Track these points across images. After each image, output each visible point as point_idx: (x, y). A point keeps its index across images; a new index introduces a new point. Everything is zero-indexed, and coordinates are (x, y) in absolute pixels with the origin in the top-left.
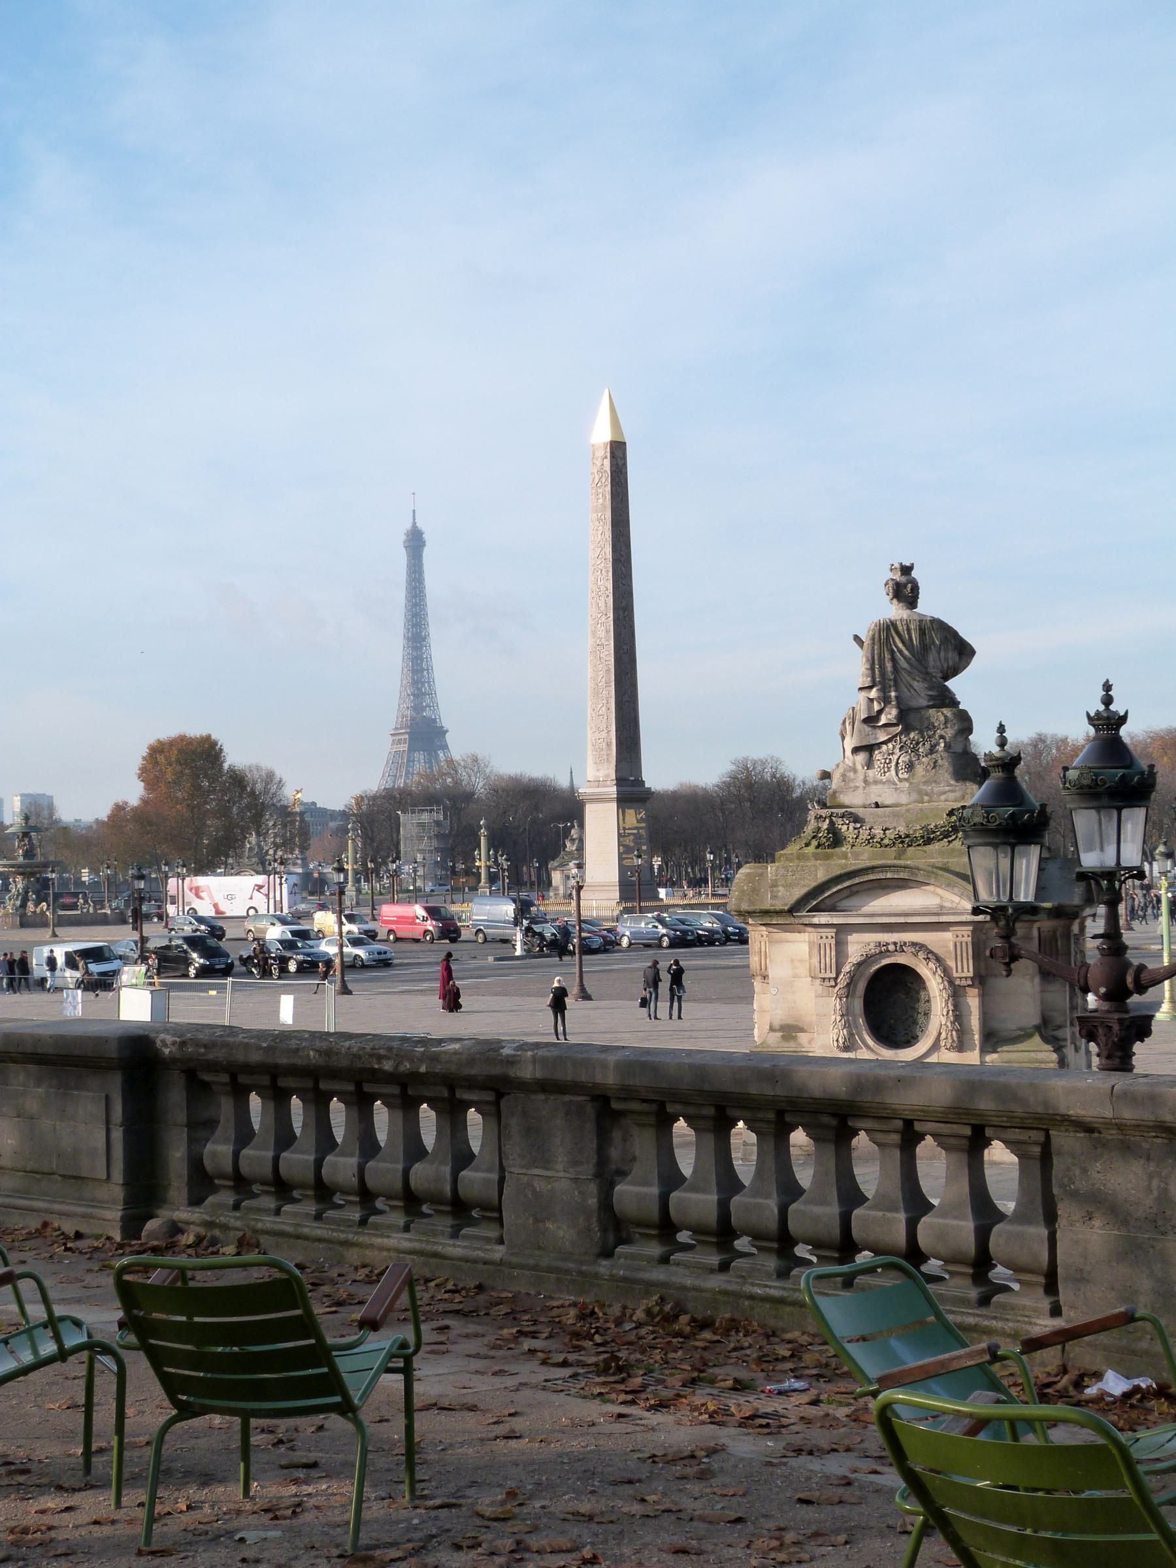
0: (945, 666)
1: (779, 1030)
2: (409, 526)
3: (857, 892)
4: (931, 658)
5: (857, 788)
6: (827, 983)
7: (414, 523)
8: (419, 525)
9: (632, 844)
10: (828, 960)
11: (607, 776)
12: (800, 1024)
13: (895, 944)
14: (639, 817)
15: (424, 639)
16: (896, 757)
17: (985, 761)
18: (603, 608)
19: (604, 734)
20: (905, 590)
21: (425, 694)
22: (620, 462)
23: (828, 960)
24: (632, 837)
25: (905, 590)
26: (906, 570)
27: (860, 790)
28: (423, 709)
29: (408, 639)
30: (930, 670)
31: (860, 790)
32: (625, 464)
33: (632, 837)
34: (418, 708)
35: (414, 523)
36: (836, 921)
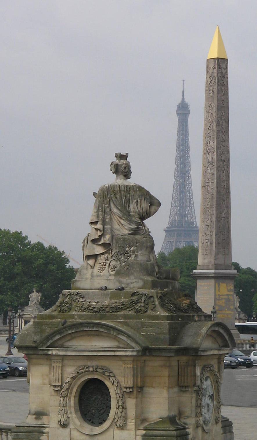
0: (141, 211)
1: (34, 414)
2: (179, 100)
3: (75, 337)
4: (132, 207)
5: (87, 279)
6: (56, 389)
7: (183, 99)
8: (187, 100)
9: (224, 305)
10: (57, 375)
11: (210, 262)
12: (45, 411)
13: (93, 367)
14: (229, 288)
15: (187, 172)
16: (108, 262)
17: (69, 266)
18: (210, 160)
19: (209, 237)
20: (122, 168)
21: (186, 207)
22: (224, 71)
23: (57, 375)
24: (224, 301)
25: (122, 168)
26: (123, 157)
27: (89, 281)
28: (186, 215)
29: (178, 171)
30: (132, 214)
31: (89, 281)
32: (227, 73)
33: (224, 301)
34: (182, 216)
35: (183, 99)
36: (61, 353)
